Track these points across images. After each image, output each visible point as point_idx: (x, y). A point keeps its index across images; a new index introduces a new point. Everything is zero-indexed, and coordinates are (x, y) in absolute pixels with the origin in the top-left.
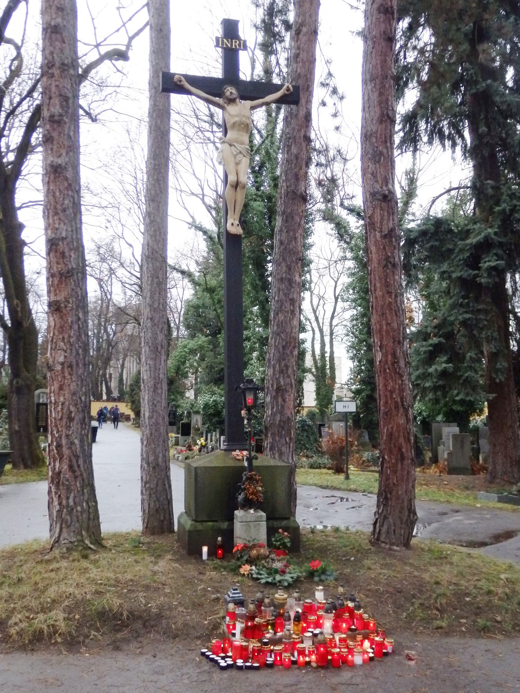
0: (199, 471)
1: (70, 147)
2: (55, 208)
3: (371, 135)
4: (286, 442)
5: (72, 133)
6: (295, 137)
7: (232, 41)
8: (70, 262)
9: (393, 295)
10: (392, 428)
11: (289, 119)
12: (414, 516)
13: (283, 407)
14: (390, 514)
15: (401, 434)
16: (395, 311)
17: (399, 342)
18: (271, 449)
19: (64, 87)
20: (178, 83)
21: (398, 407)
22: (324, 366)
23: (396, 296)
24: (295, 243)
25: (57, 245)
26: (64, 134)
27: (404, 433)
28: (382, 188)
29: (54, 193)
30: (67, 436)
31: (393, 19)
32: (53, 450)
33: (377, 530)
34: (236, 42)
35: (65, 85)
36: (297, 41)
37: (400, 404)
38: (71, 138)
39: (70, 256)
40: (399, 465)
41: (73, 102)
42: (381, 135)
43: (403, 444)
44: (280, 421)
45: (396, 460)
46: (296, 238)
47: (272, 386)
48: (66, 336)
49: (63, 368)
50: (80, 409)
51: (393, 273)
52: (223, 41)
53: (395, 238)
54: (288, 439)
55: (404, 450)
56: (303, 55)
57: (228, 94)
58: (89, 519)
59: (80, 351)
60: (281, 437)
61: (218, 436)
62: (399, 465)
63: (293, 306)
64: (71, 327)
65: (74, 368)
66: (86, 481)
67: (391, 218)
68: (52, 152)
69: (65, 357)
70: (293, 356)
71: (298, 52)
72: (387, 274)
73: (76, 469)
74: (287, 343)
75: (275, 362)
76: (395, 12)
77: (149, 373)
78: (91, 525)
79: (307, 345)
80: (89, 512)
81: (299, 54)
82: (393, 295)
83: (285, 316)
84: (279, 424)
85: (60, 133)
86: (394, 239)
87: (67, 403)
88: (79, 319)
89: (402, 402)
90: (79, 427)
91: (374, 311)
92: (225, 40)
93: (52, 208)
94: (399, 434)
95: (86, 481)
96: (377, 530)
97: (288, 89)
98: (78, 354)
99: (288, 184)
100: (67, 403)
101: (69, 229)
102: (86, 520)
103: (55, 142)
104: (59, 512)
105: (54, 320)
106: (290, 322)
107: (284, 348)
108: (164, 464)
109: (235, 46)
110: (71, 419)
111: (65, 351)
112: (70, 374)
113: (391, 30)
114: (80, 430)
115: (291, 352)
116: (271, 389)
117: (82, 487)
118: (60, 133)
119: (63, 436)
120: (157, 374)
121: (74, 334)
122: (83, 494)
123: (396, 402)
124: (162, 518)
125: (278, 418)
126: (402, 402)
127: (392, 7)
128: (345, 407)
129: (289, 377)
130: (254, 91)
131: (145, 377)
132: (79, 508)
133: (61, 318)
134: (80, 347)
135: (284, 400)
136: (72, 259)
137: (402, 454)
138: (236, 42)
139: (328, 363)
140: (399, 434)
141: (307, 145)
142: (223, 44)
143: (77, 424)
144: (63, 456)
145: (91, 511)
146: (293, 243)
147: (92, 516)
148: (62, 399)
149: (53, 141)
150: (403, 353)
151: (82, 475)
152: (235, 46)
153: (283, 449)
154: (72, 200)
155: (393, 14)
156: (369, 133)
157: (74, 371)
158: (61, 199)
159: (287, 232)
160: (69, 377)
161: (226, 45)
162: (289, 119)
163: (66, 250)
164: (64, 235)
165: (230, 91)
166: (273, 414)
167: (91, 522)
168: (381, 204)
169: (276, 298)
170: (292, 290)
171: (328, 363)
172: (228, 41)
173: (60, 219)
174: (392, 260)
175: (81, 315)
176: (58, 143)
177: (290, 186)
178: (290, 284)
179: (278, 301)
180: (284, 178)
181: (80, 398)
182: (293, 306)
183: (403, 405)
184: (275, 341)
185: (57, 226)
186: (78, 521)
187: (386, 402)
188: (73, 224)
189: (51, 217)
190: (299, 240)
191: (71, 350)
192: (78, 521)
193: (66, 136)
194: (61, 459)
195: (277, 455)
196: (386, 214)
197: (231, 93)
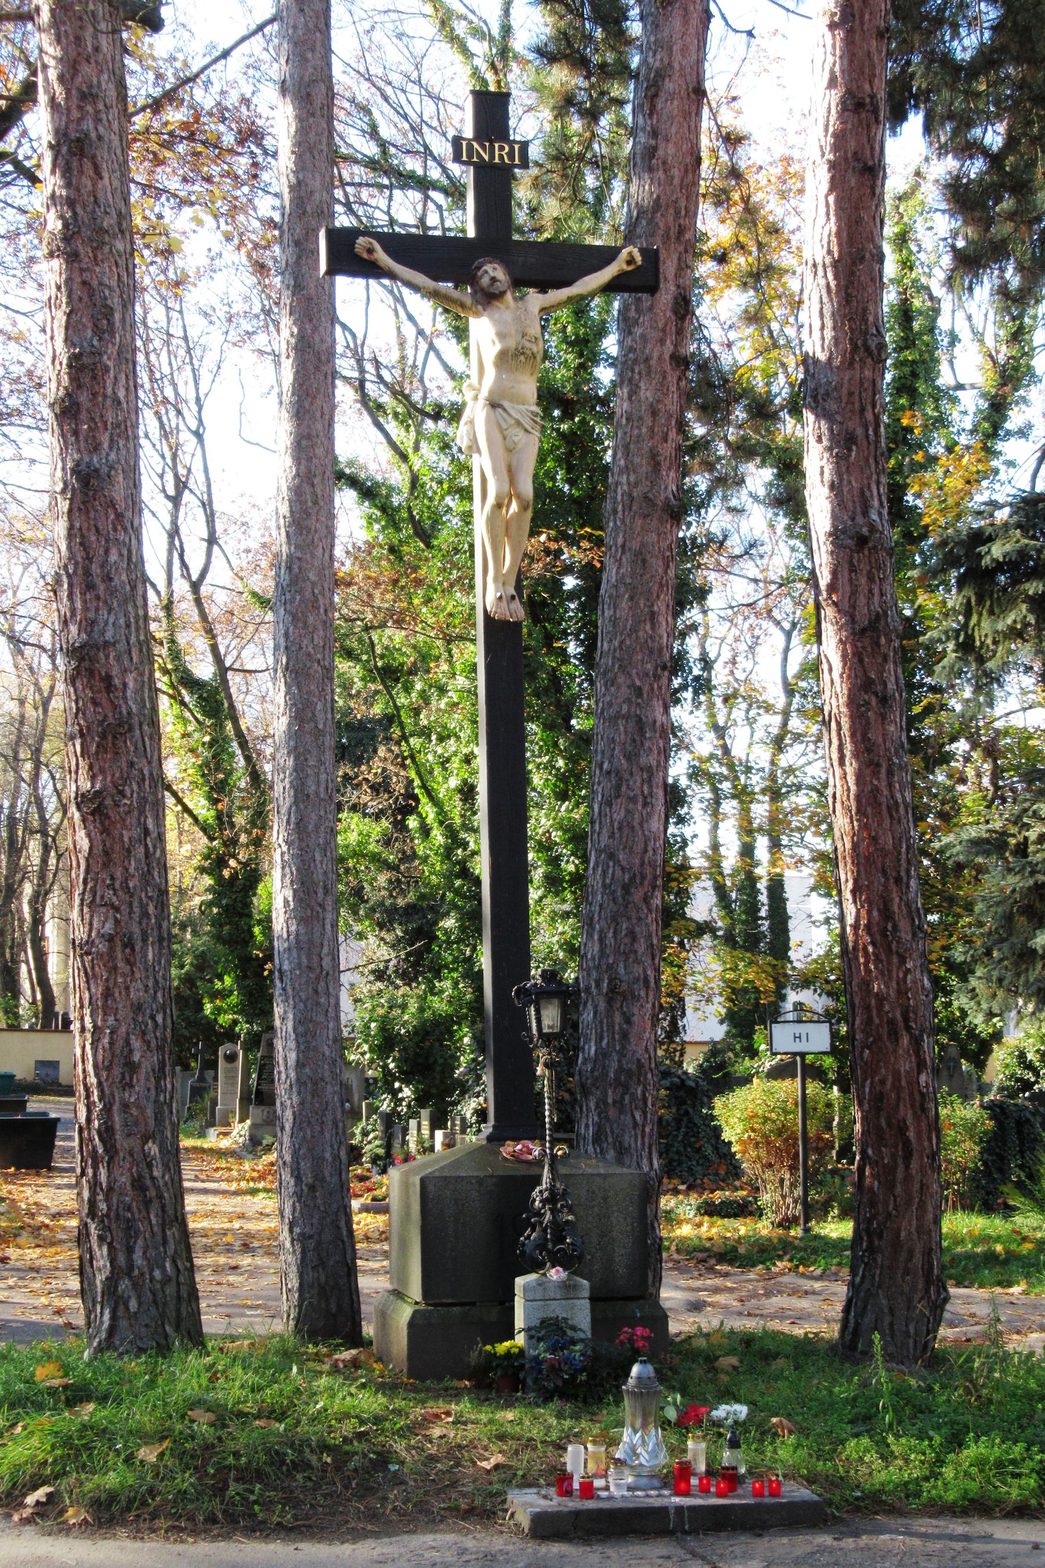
0: (431, 1188)
1: (118, 426)
2: (87, 573)
3: (827, 394)
4: (635, 1124)
5: (121, 394)
6: (647, 360)
7: (492, 148)
8: (125, 698)
9: (883, 770)
10: (883, 1082)
11: (633, 313)
12: (939, 1293)
13: (625, 1036)
14: (879, 1286)
15: (905, 1095)
16: (889, 808)
17: (898, 880)
18: (597, 1140)
19: (101, 284)
20: (365, 255)
21: (896, 1033)
22: (752, 908)
23: (890, 773)
24: (653, 628)
25: (93, 660)
26: (105, 396)
27: (911, 1094)
28: (853, 519)
29: (83, 536)
30: (125, 1106)
31: (877, 122)
32: (91, 1140)
33: (852, 1325)
34: (502, 148)
35: (106, 281)
36: (651, 115)
37: (901, 1024)
38: (119, 403)
39: (125, 685)
40: (901, 1168)
41: (123, 320)
42: (851, 394)
43: (909, 1121)
44: (620, 1070)
45: (894, 1157)
46: (653, 616)
47: (598, 985)
48: (118, 873)
49: (112, 949)
50: (153, 1044)
51: (883, 717)
52: (470, 147)
53: (886, 635)
54: (638, 1116)
55: (911, 1134)
56: (668, 150)
57: (485, 281)
58: (179, 1298)
59: (151, 909)
60: (621, 1111)
61: (426, 1132)
62: (901, 1168)
63: (650, 787)
64: (129, 851)
65: (137, 948)
66: (171, 1212)
67: (876, 591)
68: (77, 440)
69: (117, 922)
70: (650, 911)
71: (653, 142)
72: (868, 723)
73: (148, 1182)
74: (633, 878)
75: (603, 923)
76: (882, 105)
77: (295, 953)
78: (184, 1313)
79: (696, 855)
80: (178, 1284)
81: (655, 149)
82: (883, 770)
83: (628, 811)
84: (617, 1079)
85: (94, 395)
86: (883, 640)
87: (123, 1029)
88: (146, 832)
89: (906, 1020)
90: (152, 1086)
91: (838, 806)
92: (476, 145)
93: (80, 572)
94: (899, 1098)
95: (171, 1212)
96: (852, 1325)
97: (630, 261)
98: (145, 914)
99: (632, 478)
100: (123, 1029)
101: (122, 621)
102: (172, 1305)
103: (83, 415)
104: (111, 1283)
105: (88, 835)
106: (641, 824)
107: (626, 888)
108: (335, 1179)
109: (501, 157)
110: (132, 1067)
111: (117, 909)
112: (128, 962)
113: (872, 149)
114: (153, 1092)
115: (646, 899)
116: (594, 990)
117: (163, 1226)
118: (94, 395)
119: (115, 1108)
120: (315, 959)
121: (137, 869)
122: (165, 1242)
123: (892, 1022)
124: (334, 1308)
125: (613, 1065)
126: (906, 1020)
127: (873, 97)
128: (797, 1037)
129: (638, 961)
130: (551, 265)
131: (286, 967)
132: (157, 1274)
133: (105, 831)
134: (150, 898)
135: (628, 1021)
136: (129, 693)
137: (907, 1142)
138: (502, 148)
139: (763, 898)
140: (899, 1098)
141: (680, 379)
142: (470, 155)
143: (147, 1080)
144: (116, 1152)
145: (182, 1279)
146: (648, 627)
147: (184, 1294)
148: (111, 1020)
149: (78, 411)
150: (908, 906)
151: (160, 1197)
152: (501, 157)
153: (627, 1140)
154: (125, 552)
155: (875, 112)
156: (822, 391)
157: (138, 957)
158: (101, 552)
159: (631, 598)
160: (127, 969)
161: (479, 156)
162: (633, 313)
163: (115, 671)
164: (109, 635)
165: (494, 272)
166: (603, 1054)
167: (184, 1305)
168: (851, 557)
169: (606, 766)
170: (647, 744)
171: (763, 898)
172: (484, 148)
173: (98, 598)
174: (879, 688)
175: (150, 824)
176: (92, 419)
177: (636, 484)
178: (641, 730)
179: (609, 773)
180: (622, 462)
181: (153, 1018)
182: (650, 787)
183: (908, 1029)
184: (604, 872)
185: (91, 615)
186: (155, 1302)
187: (869, 1021)
188: (130, 609)
189: (77, 592)
190: (661, 619)
191: (131, 904)
192: (155, 1302)
193: (109, 402)
194: (111, 1159)
195: (611, 1154)
196: (863, 581)
197: (494, 280)
